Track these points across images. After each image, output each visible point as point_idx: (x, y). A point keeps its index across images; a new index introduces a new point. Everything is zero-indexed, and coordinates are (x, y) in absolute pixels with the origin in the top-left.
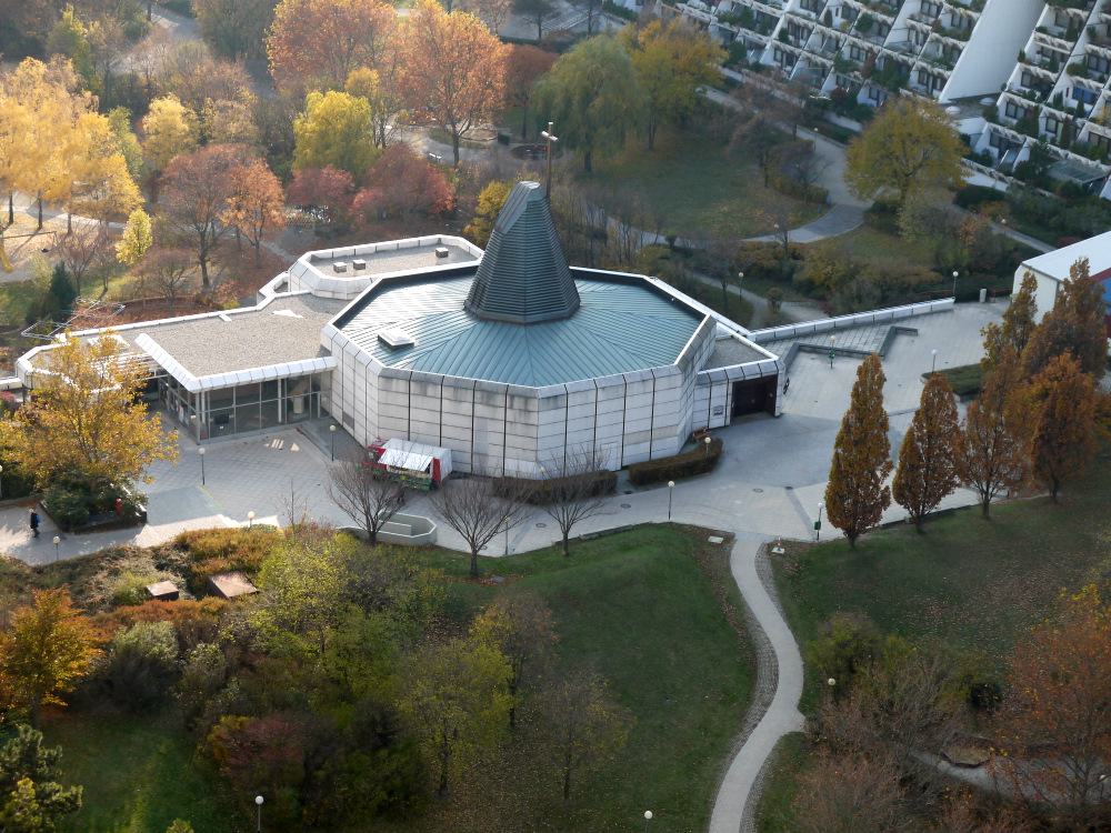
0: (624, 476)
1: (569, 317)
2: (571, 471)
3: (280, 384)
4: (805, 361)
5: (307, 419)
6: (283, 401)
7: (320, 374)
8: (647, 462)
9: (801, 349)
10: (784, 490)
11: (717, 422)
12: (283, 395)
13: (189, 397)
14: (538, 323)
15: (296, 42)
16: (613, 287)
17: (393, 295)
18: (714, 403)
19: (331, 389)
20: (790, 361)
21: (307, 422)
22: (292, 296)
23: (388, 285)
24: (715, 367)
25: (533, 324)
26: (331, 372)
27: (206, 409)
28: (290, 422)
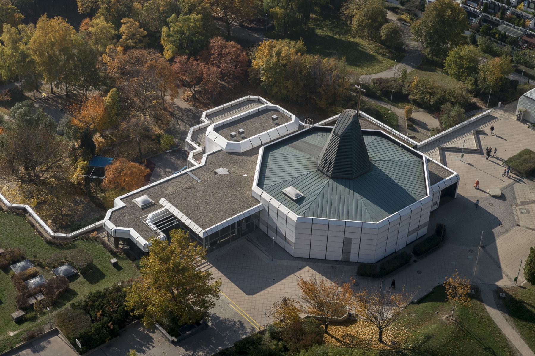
22: (214, 153)
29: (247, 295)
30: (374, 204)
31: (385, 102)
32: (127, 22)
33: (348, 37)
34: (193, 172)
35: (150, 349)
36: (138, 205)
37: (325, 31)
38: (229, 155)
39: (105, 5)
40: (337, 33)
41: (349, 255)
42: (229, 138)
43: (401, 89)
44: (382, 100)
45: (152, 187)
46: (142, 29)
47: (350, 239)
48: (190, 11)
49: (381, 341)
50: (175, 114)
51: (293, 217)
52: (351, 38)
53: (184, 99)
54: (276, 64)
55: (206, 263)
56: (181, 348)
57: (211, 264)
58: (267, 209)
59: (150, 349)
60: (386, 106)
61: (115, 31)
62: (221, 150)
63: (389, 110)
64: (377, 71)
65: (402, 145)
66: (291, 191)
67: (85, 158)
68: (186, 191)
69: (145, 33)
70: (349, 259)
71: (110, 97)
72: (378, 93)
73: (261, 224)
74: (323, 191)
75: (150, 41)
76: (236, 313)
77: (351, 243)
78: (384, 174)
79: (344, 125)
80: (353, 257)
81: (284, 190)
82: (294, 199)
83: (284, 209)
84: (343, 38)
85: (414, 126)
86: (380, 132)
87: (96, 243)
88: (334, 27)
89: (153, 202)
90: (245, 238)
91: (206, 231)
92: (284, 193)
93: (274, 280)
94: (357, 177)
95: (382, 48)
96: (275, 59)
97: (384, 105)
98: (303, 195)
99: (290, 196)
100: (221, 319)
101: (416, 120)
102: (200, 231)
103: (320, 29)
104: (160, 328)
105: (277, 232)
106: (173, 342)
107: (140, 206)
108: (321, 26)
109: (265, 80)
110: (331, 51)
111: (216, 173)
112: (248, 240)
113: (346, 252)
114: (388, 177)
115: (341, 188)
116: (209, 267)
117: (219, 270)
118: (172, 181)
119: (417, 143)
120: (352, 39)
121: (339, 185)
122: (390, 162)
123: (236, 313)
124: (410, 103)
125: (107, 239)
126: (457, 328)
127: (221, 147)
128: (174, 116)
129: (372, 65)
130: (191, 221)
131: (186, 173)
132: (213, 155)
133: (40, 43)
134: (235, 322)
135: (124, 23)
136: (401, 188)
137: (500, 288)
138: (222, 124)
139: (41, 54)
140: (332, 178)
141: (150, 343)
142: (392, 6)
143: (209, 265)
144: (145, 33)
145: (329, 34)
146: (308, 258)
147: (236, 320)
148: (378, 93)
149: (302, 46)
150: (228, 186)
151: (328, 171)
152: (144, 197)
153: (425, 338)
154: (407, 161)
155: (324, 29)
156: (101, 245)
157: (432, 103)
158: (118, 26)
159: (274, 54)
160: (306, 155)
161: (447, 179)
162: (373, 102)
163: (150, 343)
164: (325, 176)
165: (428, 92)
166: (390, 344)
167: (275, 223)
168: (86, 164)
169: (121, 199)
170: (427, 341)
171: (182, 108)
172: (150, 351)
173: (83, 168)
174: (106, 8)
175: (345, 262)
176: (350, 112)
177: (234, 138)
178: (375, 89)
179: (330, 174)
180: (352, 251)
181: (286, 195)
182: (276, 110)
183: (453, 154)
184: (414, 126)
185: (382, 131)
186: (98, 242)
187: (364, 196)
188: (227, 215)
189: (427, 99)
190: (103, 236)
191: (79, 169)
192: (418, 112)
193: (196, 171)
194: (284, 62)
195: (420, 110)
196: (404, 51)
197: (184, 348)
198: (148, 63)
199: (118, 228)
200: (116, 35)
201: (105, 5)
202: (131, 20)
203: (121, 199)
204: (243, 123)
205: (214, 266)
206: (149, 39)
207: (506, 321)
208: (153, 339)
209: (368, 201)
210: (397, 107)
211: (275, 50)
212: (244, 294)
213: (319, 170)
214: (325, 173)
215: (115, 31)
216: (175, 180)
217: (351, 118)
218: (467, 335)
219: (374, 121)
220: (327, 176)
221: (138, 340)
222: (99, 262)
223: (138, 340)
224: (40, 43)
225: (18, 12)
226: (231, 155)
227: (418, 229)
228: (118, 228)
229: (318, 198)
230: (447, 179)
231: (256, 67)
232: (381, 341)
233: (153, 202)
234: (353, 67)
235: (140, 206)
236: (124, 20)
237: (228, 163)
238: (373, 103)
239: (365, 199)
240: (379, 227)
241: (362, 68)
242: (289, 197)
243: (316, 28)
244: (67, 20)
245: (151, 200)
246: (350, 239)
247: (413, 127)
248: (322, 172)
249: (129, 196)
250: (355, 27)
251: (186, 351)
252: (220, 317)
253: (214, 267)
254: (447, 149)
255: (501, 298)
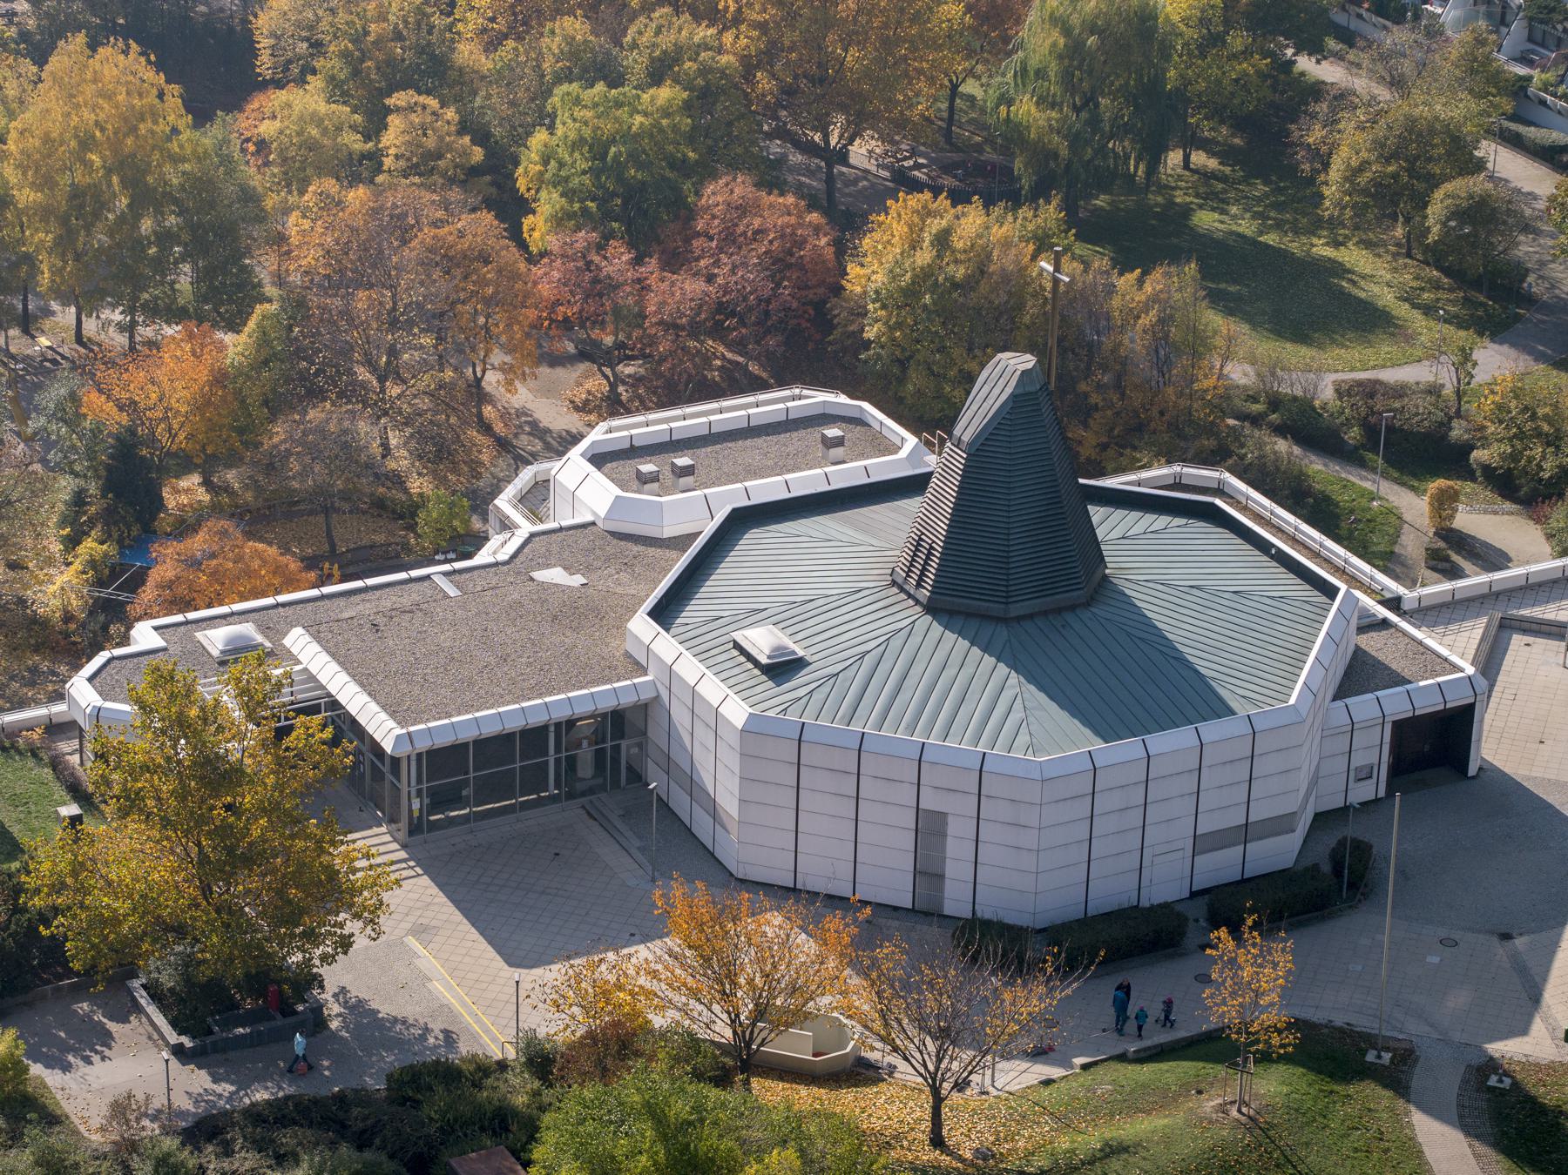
0: (1199, 910)
1: (1089, 602)
2: (1100, 904)
3: (552, 729)
4: (1517, 640)
5: (603, 788)
6: (558, 761)
7: (624, 710)
8: (1237, 883)
9: (1508, 626)
10: (1495, 940)
11: (1364, 792)
12: (558, 749)
13: (387, 761)
14: (1031, 616)
15: (603, 322)
16: (1162, 521)
17: (755, 541)
18: (1359, 760)
19: (645, 733)
20: (1490, 661)
21: (603, 796)
22: (561, 529)
23: (743, 520)
24: (1401, 807)
25: (1019, 619)
26: (646, 706)
27: (419, 781)
28: (570, 796)
29: (510, 965)
30: (1062, 707)
31: (1374, 470)
32: (411, 108)
33: (1315, 240)
34: (457, 577)
35: (91, 1063)
36: (209, 648)
37: (1234, 217)
38: (615, 541)
39: (346, 44)
40: (1279, 226)
41: (941, 889)
42: (635, 484)
43: (1446, 425)
44: (1362, 464)
45: (284, 605)
46: (467, 139)
47: (941, 818)
48: (656, 76)
49: (937, 1141)
50: (514, 447)
51: (737, 712)
52: (1327, 244)
53: (572, 402)
54: (925, 276)
55: (404, 861)
56: (203, 1072)
57: (418, 865)
58: (666, 699)
59: (91, 1063)
60: (1367, 485)
61: (367, 138)
62: (593, 524)
63: (1373, 499)
64: (1380, 362)
65: (1279, 550)
66: (762, 640)
67: (110, 536)
68: (391, 617)
69: (478, 154)
70: (941, 905)
71: (250, 337)
72: (1353, 435)
73: (650, 764)
74: (882, 648)
75: (493, 190)
76: (445, 1008)
77: (943, 835)
78: (1148, 624)
79: (986, 406)
80: (956, 901)
81: (738, 636)
82: (764, 660)
83: (712, 690)
84: (1295, 246)
85: (1455, 558)
86: (1213, 505)
87: (31, 763)
88: (1278, 206)
89: (268, 644)
90: (583, 807)
91: (409, 734)
92: (737, 646)
93: (632, 935)
94: (1031, 616)
95: (1437, 286)
96: (924, 257)
97: (1362, 478)
98: (801, 653)
99: (754, 652)
100: (380, 1015)
101: (1473, 538)
102: (384, 730)
103: (1213, 209)
104: (152, 1010)
105: (692, 785)
106: (178, 1051)
107: (215, 653)
108: (1223, 201)
109: (878, 337)
110: (1222, 286)
111: (532, 579)
112: (589, 813)
113: (928, 873)
114: (1159, 633)
115: (954, 644)
116: (411, 873)
117: (441, 887)
118: (367, 596)
119: (1401, 590)
120: (1329, 252)
121: (950, 636)
122: (1195, 591)
123: (442, 1006)
124: (1474, 480)
125: (78, 761)
126: (1244, 1138)
127: (594, 513)
128: (508, 452)
129: (1369, 342)
130: (369, 699)
131: (428, 577)
132: (554, 536)
133: (47, 139)
134: (427, 1030)
135: (398, 110)
136: (1197, 672)
137: (1491, 1058)
138: (627, 445)
139: (45, 182)
140: (931, 608)
141: (98, 1048)
142: (1548, 142)
143: (412, 868)
144: (478, 154)
145: (1247, 227)
146: (787, 889)
147: (437, 1026)
148: (1353, 435)
149: (1052, 224)
150: (555, 617)
151: (919, 585)
152: (248, 629)
153: (1101, 1150)
154: (1269, 601)
155: (1234, 210)
156: (47, 771)
157: (1547, 475)
158: (375, 124)
159: (927, 238)
160: (874, 542)
161: (1422, 683)
162: (1319, 467)
163: (98, 1048)
164: (911, 602)
165: (1539, 434)
166: (968, 1155)
167: (686, 751)
168: (106, 555)
169: (156, 628)
170: (1107, 1156)
171: (548, 431)
172: (87, 1069)
173: (92, 563)
174: (345, 55)
175: (927, 914)
176: (1012, 362)
177: (647, 487)
178: (1343, 418)
179: (924, 594)
180: (951, 870)
181: (743, 651)
182: (859, 421)
183: (1540, 643)
184: (1455, 558)
185: (1218, 502)
186: (42, 759)
187: (1031, 679)
188: (507, 698)
189: (1530, 460)
190: (68, 750)
191: (77, 565)
192: (1495, 513)
193: (467, 576)
194: (960, 272)
195: (1508, 505)
196: (1530, 300)
197: (210, 1074)
198: (427, 234)
199: (109, 705)
200: (365, 156)
201: (346, 44)
202: (433, 103)
203: (156, 628)
204: (709, 449)
205: (426, 872)
206: (493, 183)
207: (1473, 1161)
208: (113, 1039)
209: (1042, 697)
210: (1413, 489)
211: (936, 225)
212: (499, 962)
213: (894, 583)
214: (912, 592)
215: (367, 138)
216: (378, 593)
217: (1013, 382)
218: (1277, 1166)
219: (1339, 557)
220: (917, 602)
221: (62, 1034)
222: (22, 816)
223: (62, 1034)
224: (47, 139)
225: (17, 53)
226: (623, 543)
227: (1246, 833)
228: (109, 705)
229: (855, 667)
230: (1422, 683)
231: (858, 289)
232: (937, 1141)
233: (268, 644)
234: (1288, 345)
235: (215, 653)
236: (399, 99)
237: (597, 564)
238: (1318, 468)
239: (1032, 688)
240: (1046, 776)
241: (1321, 347)
242: (750, 658)
243: (1201, 207)
244: (153, 58)
245: (259, 638)
246: (941, 818)
247: (1447, 559)
248: (902, 590)
249: (187, 623)
250: (1332, 187)
251: (215, 1081)
252: (379, 1012)
253: (425, 877)
254: (1527, 625)
255: (1492, 1089)
